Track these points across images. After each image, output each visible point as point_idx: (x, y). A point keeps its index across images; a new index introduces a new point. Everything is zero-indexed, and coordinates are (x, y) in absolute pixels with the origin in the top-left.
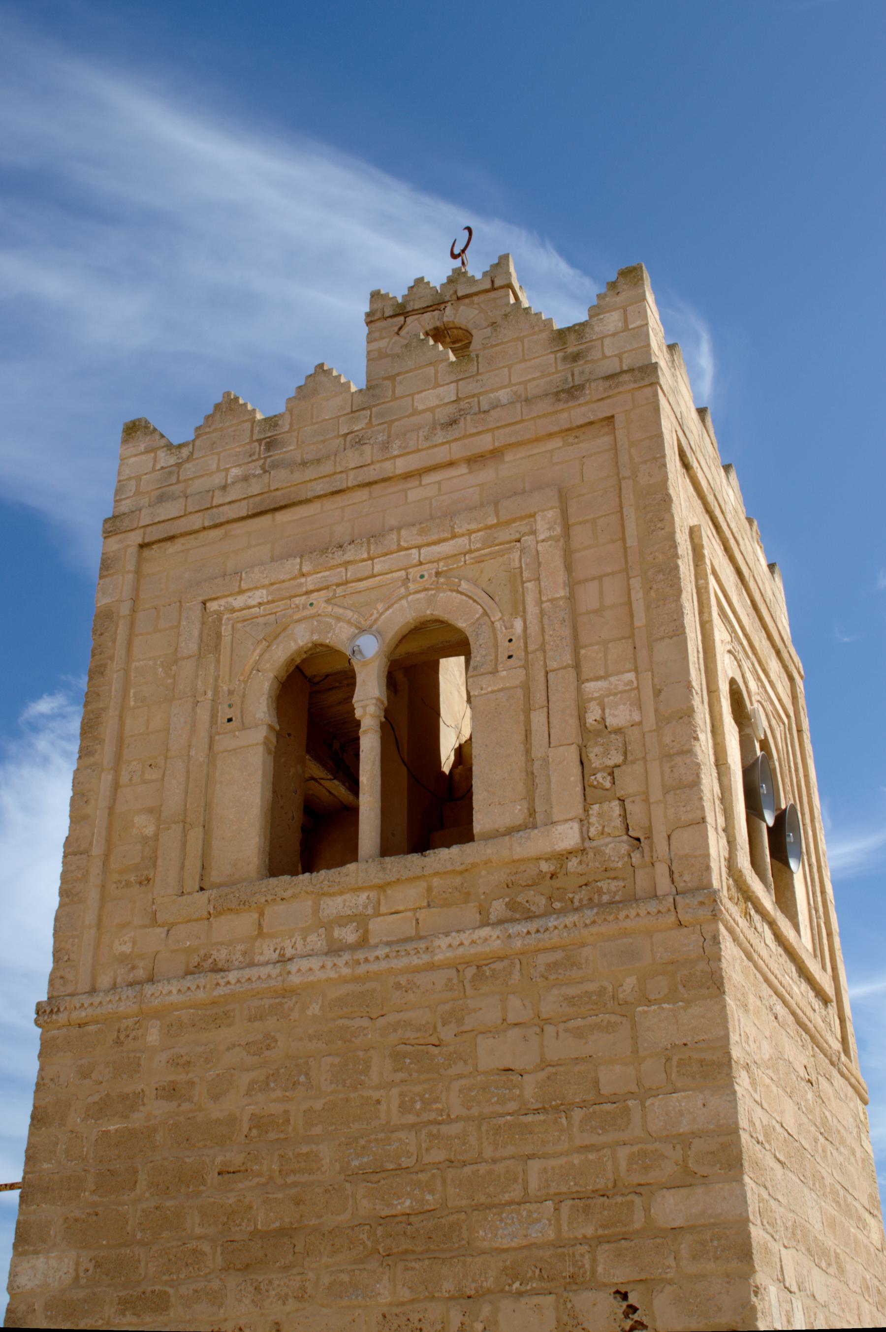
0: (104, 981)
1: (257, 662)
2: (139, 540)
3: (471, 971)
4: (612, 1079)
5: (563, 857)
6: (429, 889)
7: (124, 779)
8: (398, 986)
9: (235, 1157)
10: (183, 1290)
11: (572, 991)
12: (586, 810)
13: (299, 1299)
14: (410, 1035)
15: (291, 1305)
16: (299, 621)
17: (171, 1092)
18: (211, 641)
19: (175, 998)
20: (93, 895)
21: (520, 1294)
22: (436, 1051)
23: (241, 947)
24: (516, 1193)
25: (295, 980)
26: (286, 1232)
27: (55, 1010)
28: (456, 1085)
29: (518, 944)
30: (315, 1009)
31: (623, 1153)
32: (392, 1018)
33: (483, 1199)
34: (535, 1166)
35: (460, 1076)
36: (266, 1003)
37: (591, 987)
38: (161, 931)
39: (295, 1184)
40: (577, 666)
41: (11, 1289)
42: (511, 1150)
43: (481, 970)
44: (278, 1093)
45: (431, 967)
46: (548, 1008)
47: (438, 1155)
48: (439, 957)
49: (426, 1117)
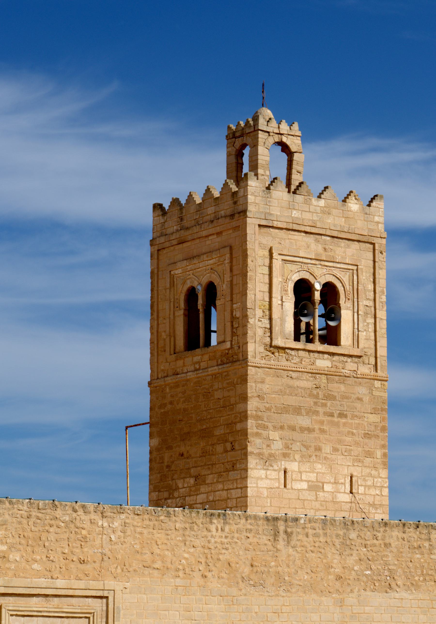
0: (160, 376)
1: (181, 290)
2: (157, 249)
3: (214, 376)
4: (233, 400)
5: (229, 349)
6: (210, 356)
7: (160, 322)
8: (204, 379)
9: (180, 417)
10: (175, 445)
11: (228, 381)
12: (232, 338)
13: (191, 446)
14: (206, 390)
15: (190, 447)
16: (188, 279)
17: (171, 403)
18: (172, 284)
19: (170, 381)
20: (156, 354)
21: (220, 444)
22: (209, 394)
23: (181, 369)
24: (219, 424)
25: (188, 377)
26: (189, 433)
27: (169, 537)
28: (212, 401)
29: (220, 371)
30: (192, 384)
31: (233, 415)
32: (203, 386)
33: (215, 425)
34: (222, 418)
35: (212, 400)
36: (184, 382)
37: (230, 380)
38: (168, 364)
39: (190, 423)
40: (232, 300)
41: (150, 446)
42: (219, 415)
43: (215, 376)
44: (187, 403)
45: (208, 375)
46: (225, 385)
47: (209, 417)
48: (209, 373)
49: (208, 408)
